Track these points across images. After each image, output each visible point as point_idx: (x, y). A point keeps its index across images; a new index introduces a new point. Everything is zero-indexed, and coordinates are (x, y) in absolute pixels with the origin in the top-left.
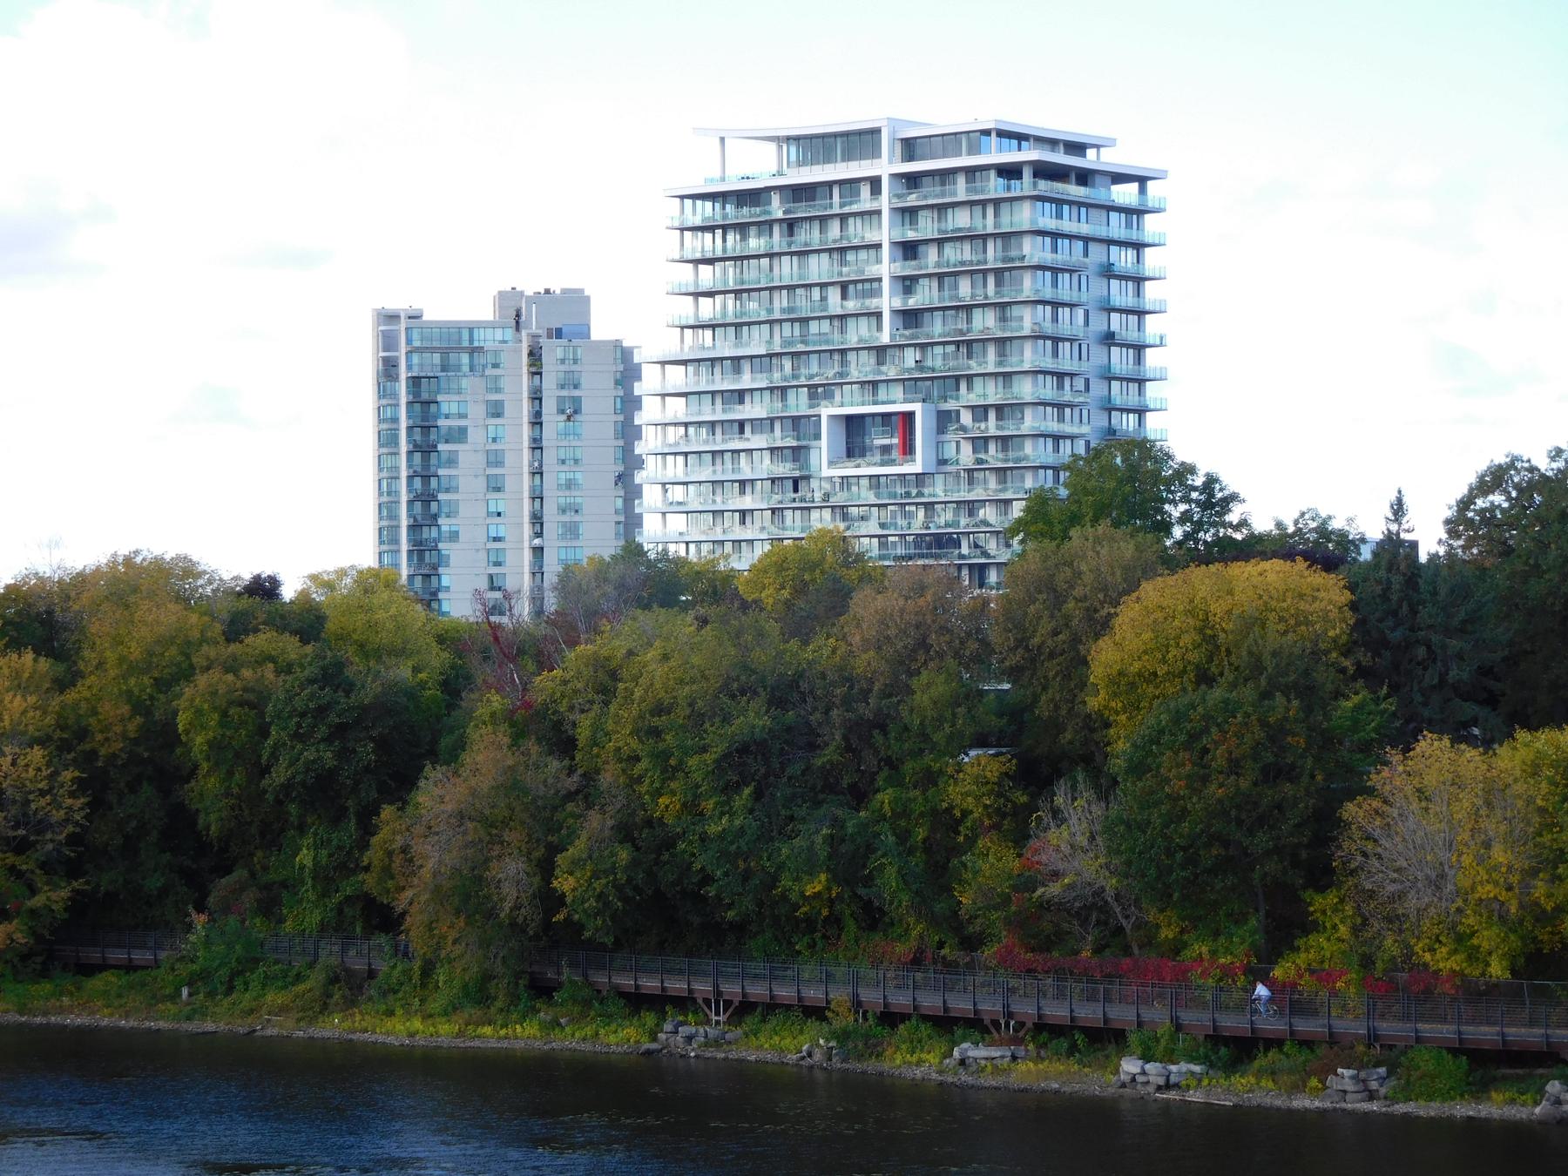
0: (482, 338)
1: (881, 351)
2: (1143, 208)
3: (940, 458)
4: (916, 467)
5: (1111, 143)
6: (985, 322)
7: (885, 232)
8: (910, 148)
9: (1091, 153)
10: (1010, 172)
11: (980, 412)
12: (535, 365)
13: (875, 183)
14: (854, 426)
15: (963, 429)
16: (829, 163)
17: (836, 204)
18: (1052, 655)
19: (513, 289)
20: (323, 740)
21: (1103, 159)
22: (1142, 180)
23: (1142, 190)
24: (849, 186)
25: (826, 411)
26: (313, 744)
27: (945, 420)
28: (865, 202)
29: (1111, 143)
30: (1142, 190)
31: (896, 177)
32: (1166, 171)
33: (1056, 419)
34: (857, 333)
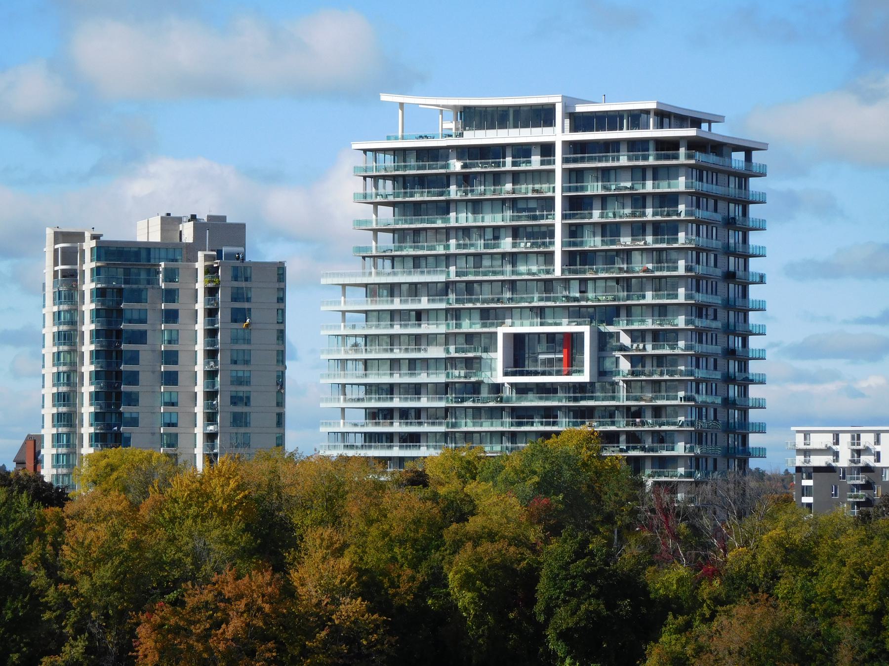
0: (157, 256)
1: (548, 285)
2: (747, 172)
3: (601, 370)
4: (585, 377)
5: (719, 119)
6: (641, 266)
7: (557, 190)
8: (579, 122)
9: (705, 126)
10: (667, 146)
11: (637, 336)
12: (213, 281)
13: (547, 149)
14: (518, 342)
15: (623, 348)
16: (480, 129)
17: (508, 164)
18: (21, 520)
19: (169, 214)
20: (593, 596)
21: (713, 130)
22: (748, 152)
23: (748, 158)
24: (523, 151)
25: (501, 331)
26: (586, 600)
27: (603, 342)
28: (536, 162)
29: (719, 119)
30: (748, 158)
31: (566, 144)
32: (767, 144)
33: (454, 327)
34: (529, 270)
